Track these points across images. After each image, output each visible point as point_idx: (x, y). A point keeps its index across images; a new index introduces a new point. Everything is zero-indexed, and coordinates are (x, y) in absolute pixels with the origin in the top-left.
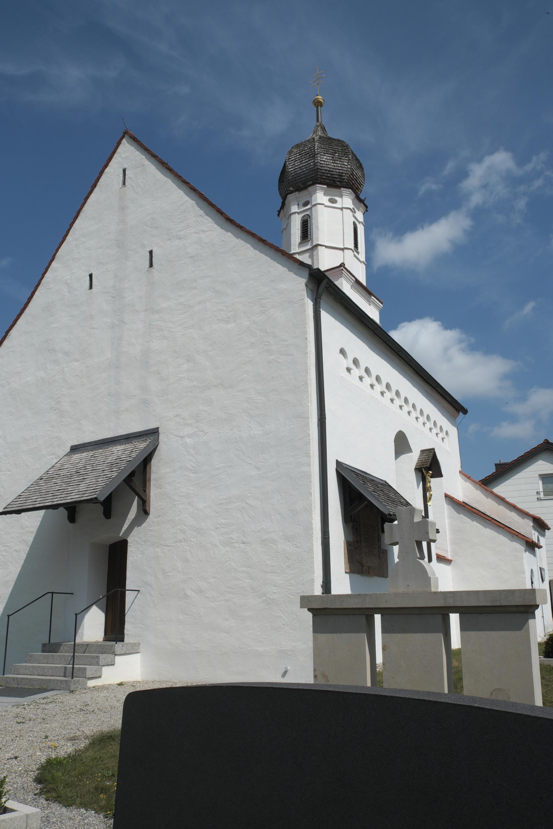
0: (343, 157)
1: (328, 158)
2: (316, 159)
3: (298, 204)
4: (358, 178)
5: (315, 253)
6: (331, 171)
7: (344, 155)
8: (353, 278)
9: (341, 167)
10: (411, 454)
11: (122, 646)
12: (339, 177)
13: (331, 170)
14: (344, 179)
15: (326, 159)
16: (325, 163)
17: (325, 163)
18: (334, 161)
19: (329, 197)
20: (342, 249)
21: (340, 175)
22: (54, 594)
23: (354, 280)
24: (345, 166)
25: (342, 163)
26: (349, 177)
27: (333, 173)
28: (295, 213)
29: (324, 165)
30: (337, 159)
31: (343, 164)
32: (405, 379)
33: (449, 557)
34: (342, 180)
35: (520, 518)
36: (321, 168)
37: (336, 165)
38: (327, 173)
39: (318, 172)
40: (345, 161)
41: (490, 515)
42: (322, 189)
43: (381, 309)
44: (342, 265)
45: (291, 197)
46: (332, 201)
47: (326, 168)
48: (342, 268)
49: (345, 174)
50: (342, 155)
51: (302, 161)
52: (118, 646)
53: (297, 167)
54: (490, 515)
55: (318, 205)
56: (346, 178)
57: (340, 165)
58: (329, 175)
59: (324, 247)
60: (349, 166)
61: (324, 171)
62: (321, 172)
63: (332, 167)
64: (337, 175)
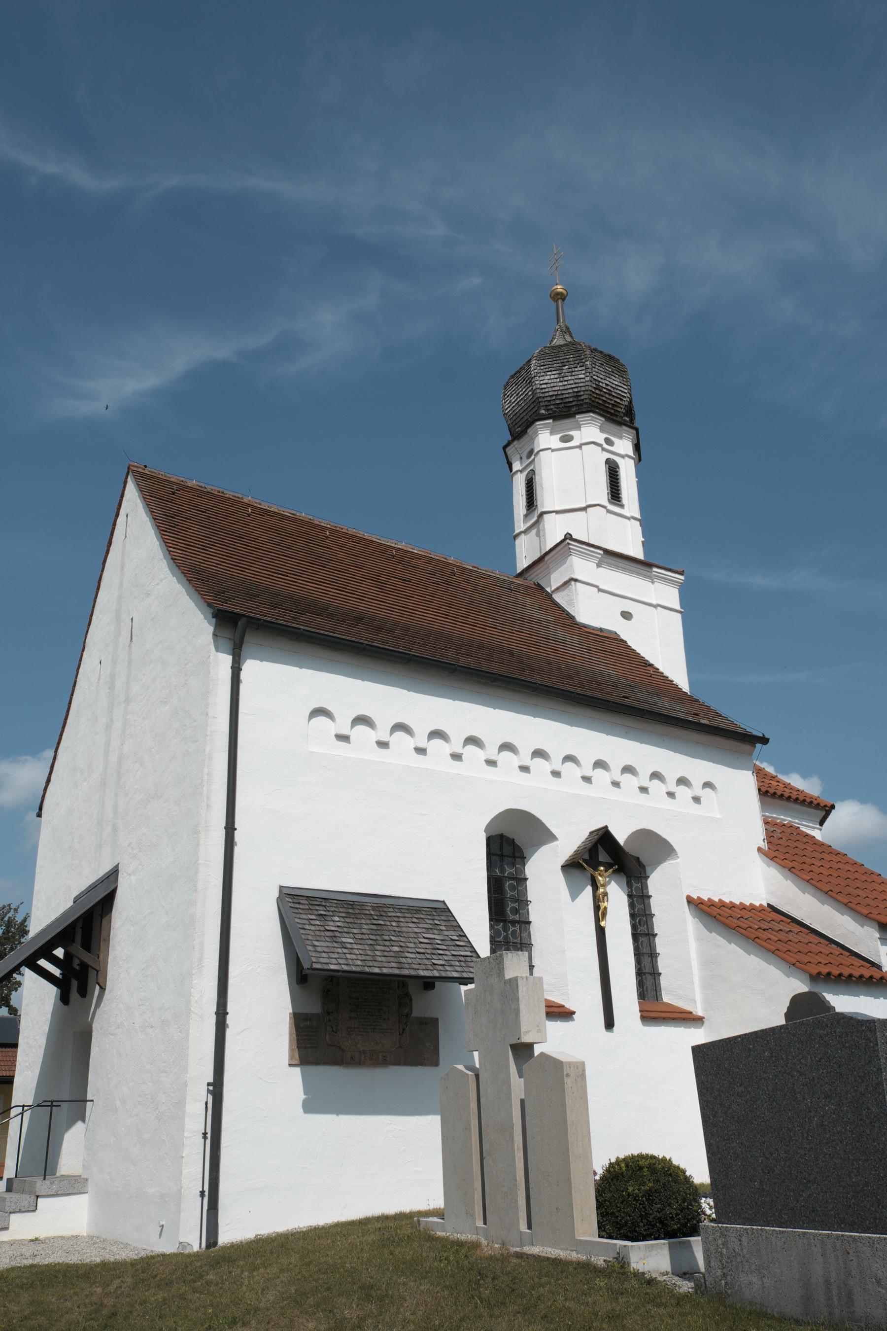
0: (576, 367)
1: (552, 377)
2: (533, 384)
3: (521, 458)
4: (612, 390)
5: (541, 526)
7: (578, 364)
8: (598, 551)
9: (575, 383)
10: (555, 843)
11: (51, 1183)
12: (575, 399)
13: (560, 393)
14: (583, 400)
15: (549, 379)
16: (549, 385)
17: (549, 385)
18: (562, 379)
19: (559, 436)
20: (584, 509)
21: (577, 395)
22: (54, 1108)
23: (602, 552)
24: (582, 380)
25: (576, 377)
26: (590, 395)
28: (517, 472)
29: (547, 390)
30: (567, 374)
31: (577, 379)
32: (538, 720)
33: (700, 1013)
35: (857, 925)
36: (543, 396)
37: (566, 383)
40: (580, 372)
42: (545, 426)
43: (681, 583)
44: (568, 536)
45: (510, 450)
46: (566, 439)
47: (551, 393)
48: (568, 541)
49: (584, 391)
50: (575, 365)
51: (519, 393)
52: (41, 1186)
53: (514, 404)
55: (541, 453)
56: (587, 397)
57: (572, 382)
58: (558, 402)
59: (554, 513)
60: (588, 379)
61: (549, 399)
62: (545, 401)
63: (561, 388)
64: (571, 397)
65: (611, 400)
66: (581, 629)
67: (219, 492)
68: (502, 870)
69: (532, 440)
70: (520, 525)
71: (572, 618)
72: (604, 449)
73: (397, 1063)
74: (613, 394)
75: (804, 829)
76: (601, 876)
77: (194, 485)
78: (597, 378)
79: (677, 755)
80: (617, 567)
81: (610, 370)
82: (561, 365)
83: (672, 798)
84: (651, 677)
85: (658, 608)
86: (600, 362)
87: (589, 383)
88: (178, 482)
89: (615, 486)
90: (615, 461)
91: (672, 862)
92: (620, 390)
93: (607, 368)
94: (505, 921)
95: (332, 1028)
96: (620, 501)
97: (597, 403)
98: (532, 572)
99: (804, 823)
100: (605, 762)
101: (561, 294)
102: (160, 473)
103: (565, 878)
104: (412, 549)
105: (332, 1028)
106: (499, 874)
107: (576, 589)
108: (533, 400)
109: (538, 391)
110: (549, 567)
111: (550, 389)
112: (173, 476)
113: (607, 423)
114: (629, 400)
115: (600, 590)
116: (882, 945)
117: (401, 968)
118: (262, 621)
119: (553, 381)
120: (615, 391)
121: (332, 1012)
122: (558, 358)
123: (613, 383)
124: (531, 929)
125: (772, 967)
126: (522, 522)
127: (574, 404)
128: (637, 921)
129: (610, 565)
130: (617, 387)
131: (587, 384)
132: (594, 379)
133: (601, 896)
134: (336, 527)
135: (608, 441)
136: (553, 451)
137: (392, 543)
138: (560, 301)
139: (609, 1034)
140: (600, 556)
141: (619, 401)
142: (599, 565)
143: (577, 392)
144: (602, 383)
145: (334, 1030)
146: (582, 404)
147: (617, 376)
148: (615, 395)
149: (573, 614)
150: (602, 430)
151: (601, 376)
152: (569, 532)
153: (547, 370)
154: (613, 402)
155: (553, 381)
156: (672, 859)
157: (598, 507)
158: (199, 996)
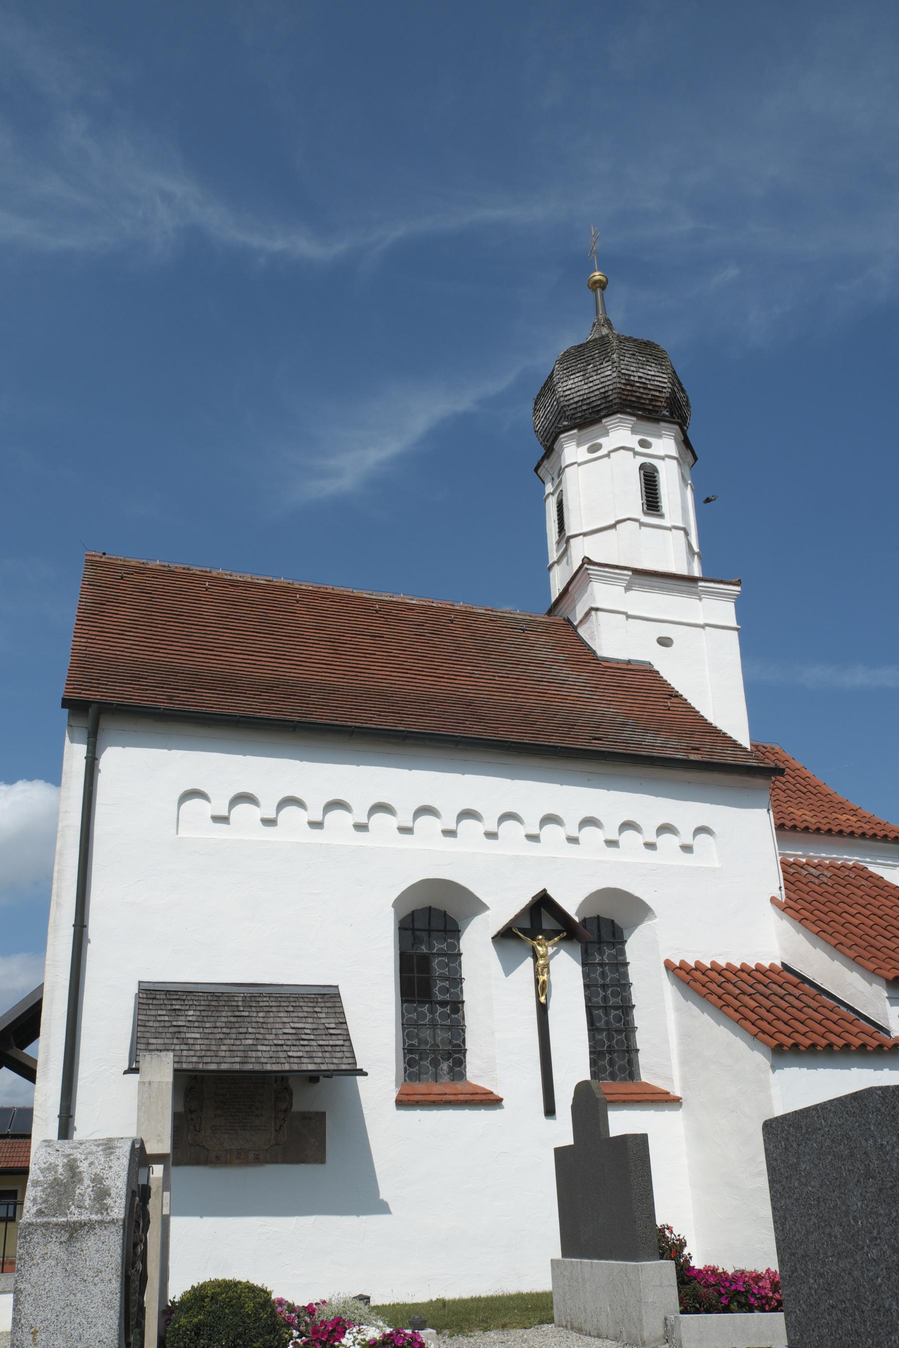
0: (602, 364)
1: (576, 380)
3: (553, 479)
4: (647, 382)
6: (585, 399)
7: (604, 359)
9: (602, 383)
10: (488, 912)
12: (603, 401)
13: (585, 397)
14: (612, 401)
15: (573, 384)
16: (573, 391)
17: (573, 391)
18: (586, 381)
19: (587, 446)
20: (613, 526)
21: (605, 396)
23: (630, 573)
24: (609, 378)
25: (602, 375)
26: (620, 393)
27: (591, 400)
28: (549, 494)
29: (571, 396)
33: (677, 1092)
34: (610, 404)
37: (591, 385)
38: (581, 406)
39: (565, 412)
40: (606, 369)
41: (822, 984)
42: (571, 438)
43: (737, 595)
45: (541, 472)
47: (576, 399)
48: (586, 566)
49: (612, 390)
54: (822, 984)
57: (598, 382)
58: (585, 407)
60: (615, 375)
61: (574, 406)
63: (587, 391)
64: (598, 400)
65: (647, 394)
66: (600, 664)
67: (184, 569)
68: (430, 947)
69: (560, 456)
70: (553, 555)
71: (594, 652)
72: (636, 453)
73: (274, 1161)
74: (649, 387)
75: (872, 869)
76: (541, 945)
77: (156, 566)
78: (626, 372)
79: (660, 799)
80: (652, 587)
81: (644, 359)
82: (585, 364)
83: (652, 850)
84: (669, 710)
85: (707, 628)
86: (631, 352)
87: (617, 380)
88: (139, 565)
89: (652, 494)
90: (652, 465)
91: (650, 923)
92: (658, 381)
93: (641, 358)
94: (430, 1002)
95: (195, 1127)
96: (658, 511)
97: (630, 400)
98: (561, 606)
99: (878, 861)
100: (557, 816)
101: (600, 281)
102: (119, 558)
103: (495, 949)
104: (411, 599)
105: (195, 1127)
106: (425, 951)
107: (597, 619)
108: (558, 411)
109: (562, 399)
110: (574, 598)
111: (575, 395)
112: (132, 559)
113: (639, 422)
114: (670, 390)
115: (628, 617)
116: (892, 1005)
117: (245, 1063)
118: (115, 705)
119: (577, 384)
120: (652, 382)
121: (195, 1111)
122: (582, 357)
123: (648, 375)
124: (465, 1010)
125: (738, 1039)
126: (555, 551)
127: (602, 407)
128: (609, 992)
129: (642, 586)
130: (653, 378)
131: (614, 380)
132: (622, 373)
133: (539, 969)
134: (319, 588)
135: (644, 444)
136: (579, 465)
137: (386, 597)
138: (599, 290)
139: (550, 1122)
140: (628, 578)
141: (657, 394)
142: (628, 589)
143: (604, 393)
144: (634, 376)
145: (197, 1128)
146: (611, 406)
147: (653, 365)
148: (652, 388)
149: (594, 648)
150: (634, 431)
151: (632, 369)
152: (587, 556)
153: (570, 373)
154: (650, 397)
155: (577, 384)
156: (650, 919)
157: (629, 521)
158: (43, 1099)
